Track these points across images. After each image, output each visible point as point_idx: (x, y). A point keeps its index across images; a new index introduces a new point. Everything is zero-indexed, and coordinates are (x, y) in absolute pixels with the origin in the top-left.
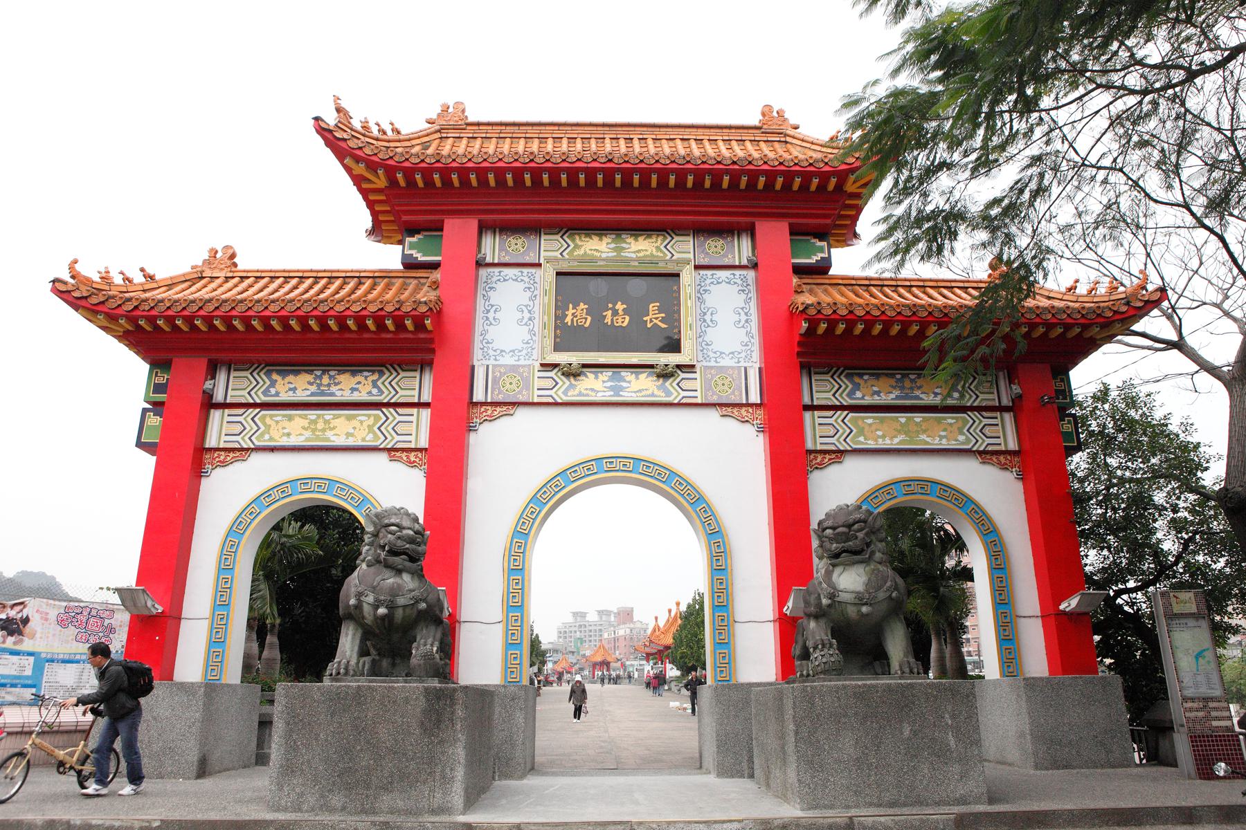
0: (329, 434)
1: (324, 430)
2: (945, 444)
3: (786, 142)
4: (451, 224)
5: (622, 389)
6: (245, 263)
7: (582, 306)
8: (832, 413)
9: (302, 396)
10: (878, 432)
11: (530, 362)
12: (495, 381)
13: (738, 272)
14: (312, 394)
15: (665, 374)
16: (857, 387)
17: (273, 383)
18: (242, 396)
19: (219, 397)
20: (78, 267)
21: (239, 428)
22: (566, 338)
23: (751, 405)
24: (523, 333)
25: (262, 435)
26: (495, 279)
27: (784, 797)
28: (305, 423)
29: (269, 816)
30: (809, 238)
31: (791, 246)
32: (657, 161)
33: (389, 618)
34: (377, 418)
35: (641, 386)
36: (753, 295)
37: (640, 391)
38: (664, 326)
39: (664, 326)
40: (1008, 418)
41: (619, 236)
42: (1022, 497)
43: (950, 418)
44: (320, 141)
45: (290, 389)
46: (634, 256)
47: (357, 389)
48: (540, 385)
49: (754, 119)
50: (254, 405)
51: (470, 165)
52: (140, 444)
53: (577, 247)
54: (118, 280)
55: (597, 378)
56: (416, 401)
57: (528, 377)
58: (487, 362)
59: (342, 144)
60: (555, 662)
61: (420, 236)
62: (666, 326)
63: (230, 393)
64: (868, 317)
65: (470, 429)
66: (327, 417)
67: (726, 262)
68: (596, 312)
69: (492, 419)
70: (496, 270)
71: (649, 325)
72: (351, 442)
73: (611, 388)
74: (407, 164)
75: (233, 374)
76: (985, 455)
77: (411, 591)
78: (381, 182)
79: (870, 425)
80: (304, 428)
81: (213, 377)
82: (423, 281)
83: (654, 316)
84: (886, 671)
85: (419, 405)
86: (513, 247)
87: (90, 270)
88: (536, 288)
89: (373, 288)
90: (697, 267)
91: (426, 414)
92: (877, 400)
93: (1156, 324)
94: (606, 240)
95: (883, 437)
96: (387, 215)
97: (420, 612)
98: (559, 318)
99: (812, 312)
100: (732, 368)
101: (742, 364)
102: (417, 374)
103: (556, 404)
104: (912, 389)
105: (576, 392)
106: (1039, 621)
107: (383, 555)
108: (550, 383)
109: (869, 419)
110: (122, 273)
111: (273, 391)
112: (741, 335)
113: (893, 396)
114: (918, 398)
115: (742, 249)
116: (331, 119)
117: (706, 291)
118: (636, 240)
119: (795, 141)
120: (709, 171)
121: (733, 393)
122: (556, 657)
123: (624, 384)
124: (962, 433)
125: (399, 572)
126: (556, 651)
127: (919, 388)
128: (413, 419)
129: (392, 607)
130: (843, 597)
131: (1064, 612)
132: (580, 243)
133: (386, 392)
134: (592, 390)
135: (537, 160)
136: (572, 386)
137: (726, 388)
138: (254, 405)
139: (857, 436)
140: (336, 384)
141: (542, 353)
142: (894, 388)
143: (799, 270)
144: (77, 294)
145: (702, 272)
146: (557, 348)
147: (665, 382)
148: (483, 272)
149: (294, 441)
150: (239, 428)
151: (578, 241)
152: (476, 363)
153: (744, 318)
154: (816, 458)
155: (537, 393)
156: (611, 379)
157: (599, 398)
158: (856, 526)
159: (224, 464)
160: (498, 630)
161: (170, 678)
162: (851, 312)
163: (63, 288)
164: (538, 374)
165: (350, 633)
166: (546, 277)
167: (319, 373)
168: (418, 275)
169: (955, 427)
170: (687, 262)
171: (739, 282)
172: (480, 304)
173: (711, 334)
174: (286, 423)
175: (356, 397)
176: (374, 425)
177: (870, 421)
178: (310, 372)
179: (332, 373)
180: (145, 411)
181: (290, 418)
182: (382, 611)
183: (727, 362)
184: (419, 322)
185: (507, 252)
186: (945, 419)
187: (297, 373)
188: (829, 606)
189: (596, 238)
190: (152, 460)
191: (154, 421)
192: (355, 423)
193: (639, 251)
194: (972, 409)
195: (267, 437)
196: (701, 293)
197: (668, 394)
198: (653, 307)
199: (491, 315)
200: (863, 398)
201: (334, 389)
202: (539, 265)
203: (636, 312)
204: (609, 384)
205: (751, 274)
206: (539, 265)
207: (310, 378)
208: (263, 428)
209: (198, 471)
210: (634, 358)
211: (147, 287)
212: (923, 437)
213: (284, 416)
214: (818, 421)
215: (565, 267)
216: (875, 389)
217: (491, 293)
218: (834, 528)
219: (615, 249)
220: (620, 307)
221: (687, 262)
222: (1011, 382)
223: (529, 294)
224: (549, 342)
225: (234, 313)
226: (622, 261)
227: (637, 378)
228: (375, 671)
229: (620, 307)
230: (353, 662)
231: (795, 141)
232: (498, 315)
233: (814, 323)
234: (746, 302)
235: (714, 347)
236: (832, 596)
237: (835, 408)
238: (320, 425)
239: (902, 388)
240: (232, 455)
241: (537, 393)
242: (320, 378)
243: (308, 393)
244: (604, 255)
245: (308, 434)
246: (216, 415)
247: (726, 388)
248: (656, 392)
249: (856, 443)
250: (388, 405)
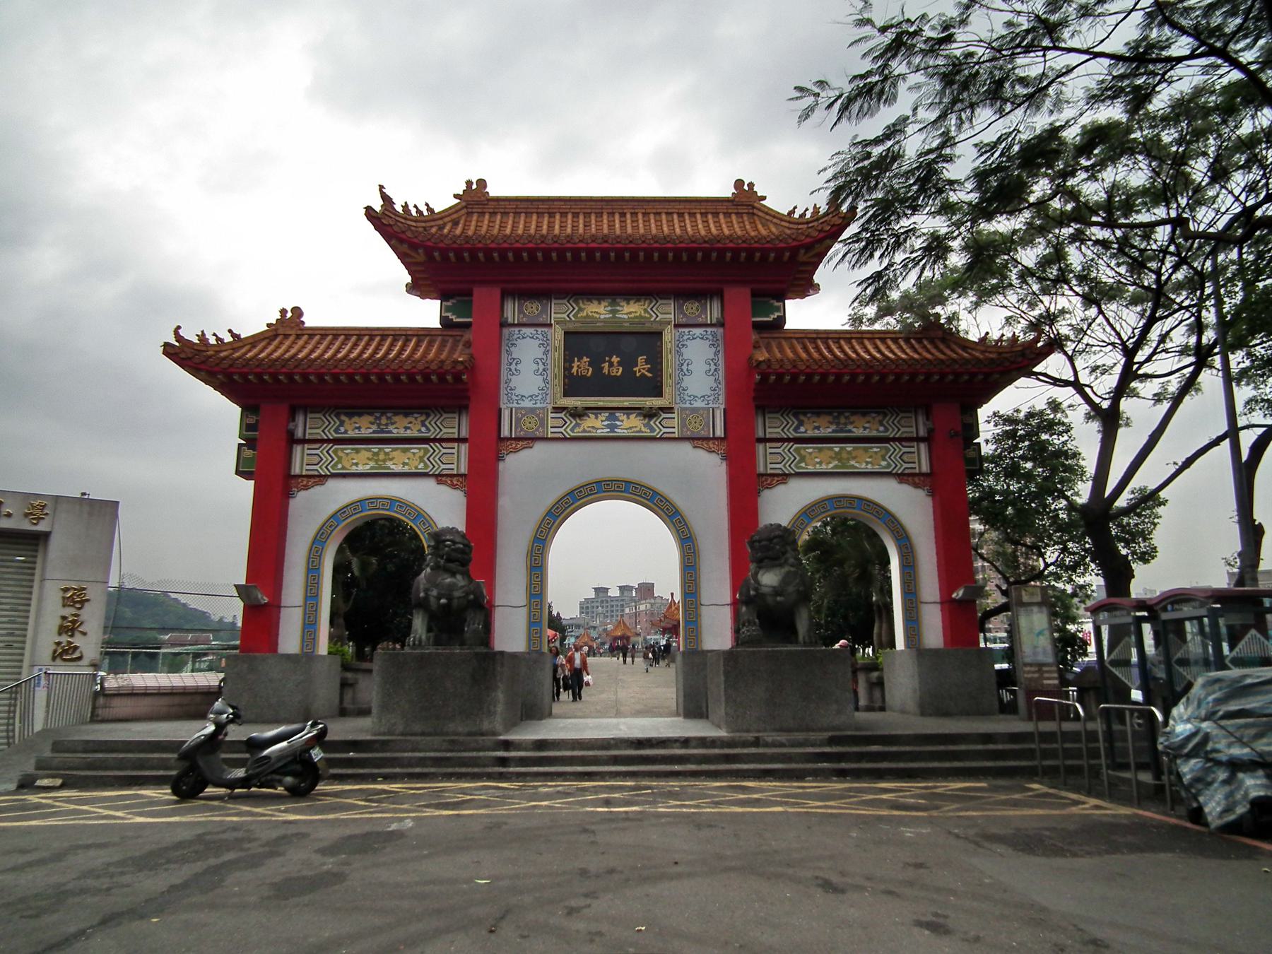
0: (389, 464)
1: (384, 461)
2: (870, 468)
3: (753, 214)
4: (479, 292)
5: (617, 426)
6: (310, 321)
7: (585, 359)
8: (780, 444)
9: (366, 432)
10: (817, 458)
11: (545, 405)
12: (518, 420)
13: (709, 330)
14: (374, 432)
15: (650, 414)
16: (801, 423)
17: (342, 423)
18: (318, 433)
19: (299, 434)
20: (181, 332)
21: (316, 459)
22: (573, 386)
23: (714, 438)
24: (539, 381)
25: (336, 465)
26: (516, 336)
27: (719, 727)
28: (369, 455)
29: (374, 738)
30: (766, 299)
31: (753, 302)
32: (644, 242)
33: (448, 606)
34: (426, 451)
35: (630, 424)
36: (721, 348)
37: (631, 428)
38: (650, 375)
39: (650, 375)
40: (923, 447)
41: (614, 300)
42: (931, 510)
43: (875, 448)
44: (369, 226)
45: (356, 428)
46: (626, 317)
47: (409, 428)
48: (553, 424)
49: (728, 191)
50: (328, 441)
51: (493, 245)
52: (238, 473)
53: (581, 310)
54: (213, 341)
55: (597, 418)
56: (456, 436)
57: (543, 419)
58: (511, 405)
59: (389, 229)
60: (577, 637)
61: (454, 301)
62: (1106, 495)
63: (308, 431)
64: (808, 370)
65: (499, 458)
66: (387, 450)
67: (700, 320)
68: (596, 363)
69: (516, 451)
70: (516, 330)
71: (638, 375)
72: (406, 469)
73: (608, 426)
74: (441, 245)
75: (309, 416)
76: (440, 478)
77: (462, 587)
78: (421, 256)
79: (810, 454)
80: (368, 459)
81: (294, 420)
82: (458, 338)
83: (642, 367)
84: (796, 642)
85: (460, 440)
86: (530, 310)
87: (191, 335)
88: (548, 345)
89: (417, 345)
90: (676, 326)
91: (464, 448)
92: (816, 433)
93: (1054, 364)
94: (604, 304)
95: (820, 463)
96: (542, 778)
97: (469, 601)
98: (568, 369)
99: (764, 366)
100: (703, 409)
101: (711, 405)
102: (456, 416)
103: (565, 439)
104: (846, 424)
105: (581, 429)
106: (938, 607)
107: (442, 562)
108: (561, 422)
109: (810, 449)
110: (215, 335)
111: (342, 429)
112: (711, 381)
113: (830, 430)
114: (850, 431)
115: (714, 311)
116: (377, 205)
117: (683, 345)
118: (628, 304)
119: (760, 214)
120: (686, 249)
121: (703, 429)
122: (577, 632)
123: (618, 423)
124: (884, 459)
125: (453, 574)
126: (578, 626)
127: (852, 423)
128: (455, 451)
129: (450, 599)
130: (764, 590)
131: (954, 600)
132: (583, 306)
133: (433, 430)
134: (593, 427)
135: (547, 241)
136: (577, 425)
137: (697, 425)
138: (328, 441)
139: (800, 462)
140: (392, 424)
141: (554, 399)
142: (831, 423)
143: (759, 327)
144: (183, 356)
145: (681, 330)
146: (566, 394)
147: (650, 420)
148: (506, 331)
149: (361, 469)
150: (316, 459)
151: (581, 305)
152: (502, 406)
153: (713, 367)
154: (766, 480)
155: (550, 430)
156: (607, 419)
157: (599, 433)
158: (775, 541)
159: (306, 488)
160: (523, 613)
161: (275, 650)
162: (795, 367)
163: (171, 351)
164: (550, 415)
165: (420, 619)
166: (557, 335)
167: (378, 415)
168: (455, 333)
169: (879, 454)
170: (669, 323)
171: (710, 337)
172: (504, 358)
173: (687, 381)
174: (354, 455)
175: (409, 434)
176: (424, 456)
177: (810, 450)
178: (371, 414)
179: (389, 415)
180: (240, 445)
181: (357, 451)
182: (443, 601)
183: (699, 404)
184: (457, 377)
185: (525, 314)
186: (871, 448)
187: (360, 415)
188: (755, 596)
189: (596, 302)
190: (251, 484)
191: (248, 453)
192: (409, 455)
193: (630, 313)
194: (894, 439)
195: (340, 466)
196: (680, 346)
197: (652, 430)
198: (641, 359)
199: (513, 367)
200: (805, 432)
201: (391, 428)
202: (550, 325)
203: (628, 363)
204: (606, 423)
205: (720, 331)
206: (550, 325)
207: (371, 419)
208: (336, 459)
209: (287, 495)
210: (626, 402)
211: (235, 346)
212: (853, 463)
213: (352, 449)
214: (769, 451)
215: (571, 327)
216: (816, 424)
217: (513, 349)
218: (759, 541)
219: (611, 312)
220: (615, 359)
221: (669, 323)
222: (928, 419)
223: (543, 349)
224: (560, 390)
225: (310, 370)
226: (616, 322)
227: (628, 418)
228: (437, 643)
229: (615, 359)
230: (424, 637)
231: (760, 214)
232: (519, 367)
233: (765, 377)
234: (715, 354)
235: (689, 392)
236: (756, 590)
237: (782, 440)
238: (382, 457)
239: (838, 424)
240: (313, 480)
241: (550, 430)
242: (379, 418)
243: (371, 431)
244: (602, 317)
245: (372, 464)
246: (298, 450)
247: (697, 425)
248: (643, 429)
249: (798, 468)
250: (435, 440)
